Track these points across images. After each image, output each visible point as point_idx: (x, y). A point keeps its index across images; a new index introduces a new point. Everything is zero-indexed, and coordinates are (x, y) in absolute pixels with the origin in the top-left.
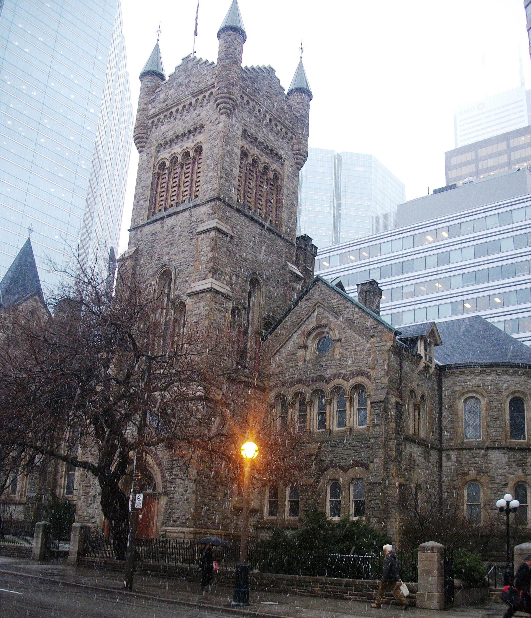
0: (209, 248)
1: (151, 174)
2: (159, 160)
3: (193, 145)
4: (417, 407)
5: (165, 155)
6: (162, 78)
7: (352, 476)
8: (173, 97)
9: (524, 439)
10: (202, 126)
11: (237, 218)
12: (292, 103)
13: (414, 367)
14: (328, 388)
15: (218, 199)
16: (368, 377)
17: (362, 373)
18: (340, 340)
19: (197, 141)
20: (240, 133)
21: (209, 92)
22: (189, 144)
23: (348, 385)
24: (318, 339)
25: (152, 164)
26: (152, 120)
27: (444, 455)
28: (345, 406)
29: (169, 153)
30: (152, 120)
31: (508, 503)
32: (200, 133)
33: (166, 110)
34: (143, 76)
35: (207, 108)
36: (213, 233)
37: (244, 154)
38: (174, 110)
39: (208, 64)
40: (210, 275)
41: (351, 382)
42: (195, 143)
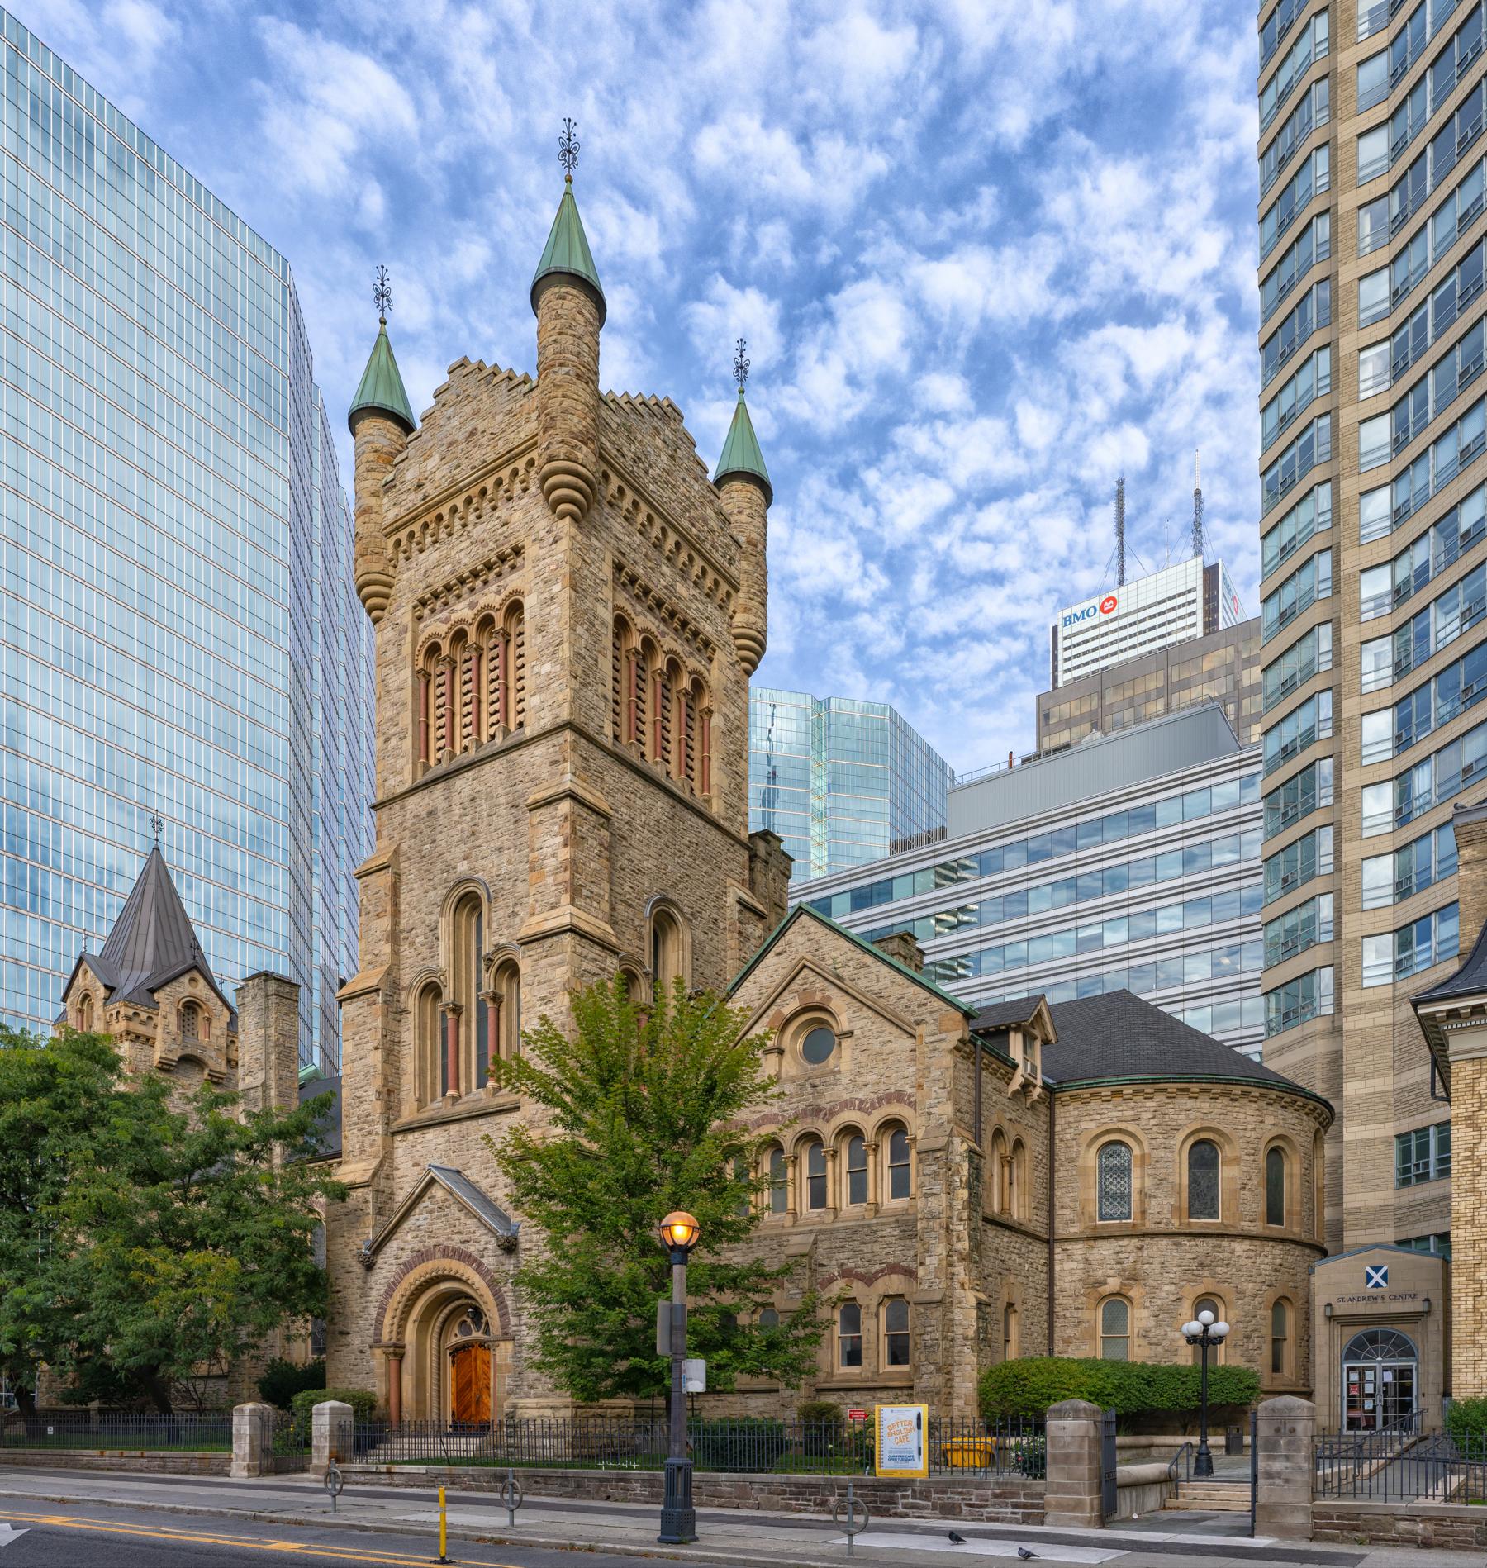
0: (560, 839)
1: (407, 674)
2: (422, 639)
3: (499, 599)
4: (1006, 1162)
5: (437, 626)
6: (406, 426)
7: (882, 1292)
8: (438, 475)
9: (1214, 1215)
10: (518, 551)
11: (615, 775)
12: (726, 509)
13: (1001, 1085)
14: (827, 1130)
15: (568, 725)
16: (912, 1105)
17: (899, 1097)
18: (851, 1033)
19: (510, 589)
20: (607, 571)
21: (525, 459)
22: (491, 598)
23: (869, 1123)
24: (813, 1028)
25: (407, 648)
26: (394, 539)
27: (1057, 1250)
28: (865, 1163)
29: (446, 621)
30: (394, 539)
31: (1206, 1327)
32: (513, 567)
33: (428, 510)
34: (354, 419)
35: (523, 502)
36: (565, 807)
37: (622, 624)
38: (445, 510)
39: (516, 381)
40: (565, 898)
41: (878, 1116)
42: (505, 593)
